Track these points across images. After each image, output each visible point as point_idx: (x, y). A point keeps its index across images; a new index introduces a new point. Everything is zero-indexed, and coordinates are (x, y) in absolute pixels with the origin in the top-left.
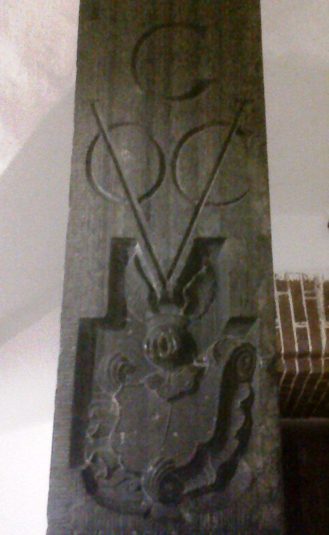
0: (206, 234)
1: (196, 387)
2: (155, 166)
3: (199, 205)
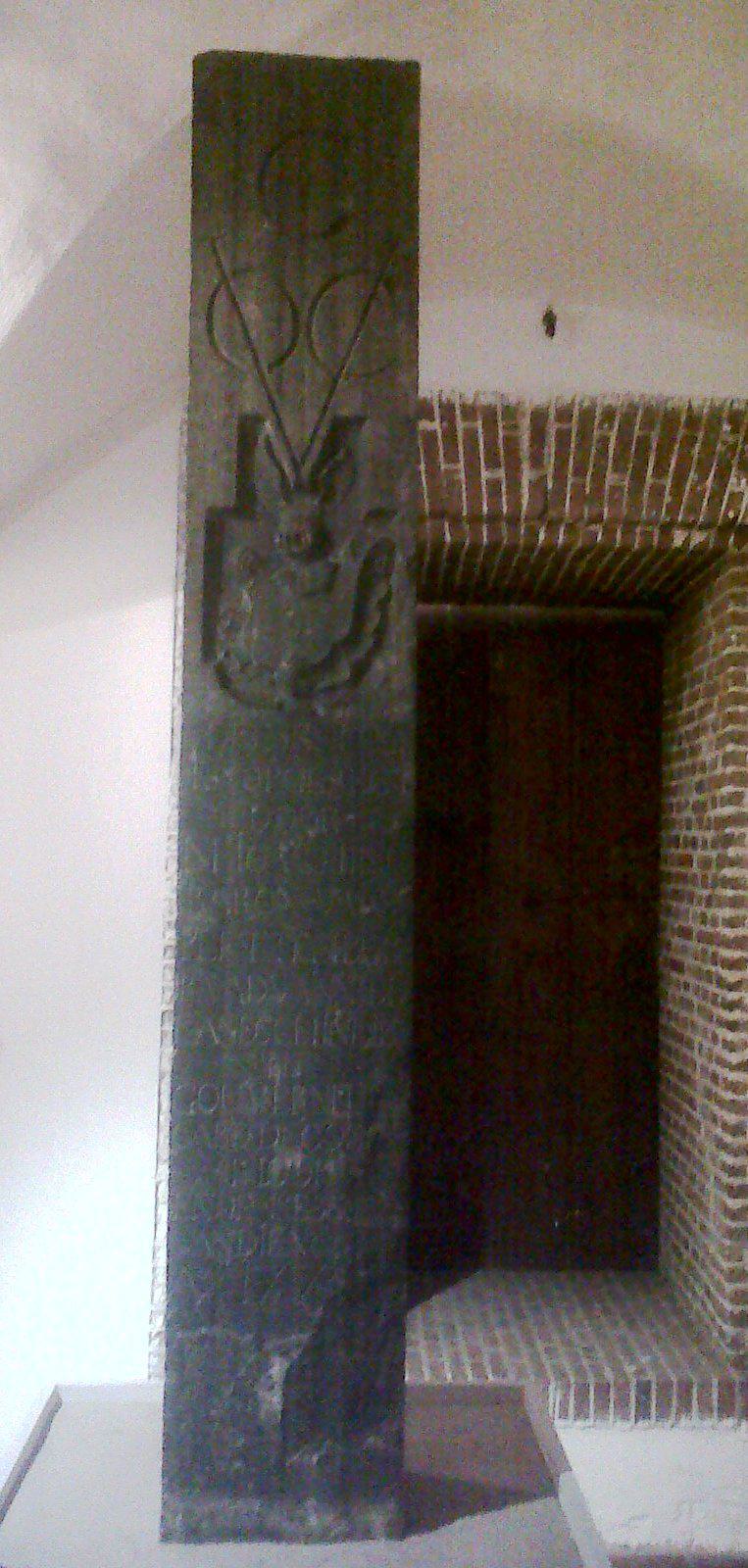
0: (345, 412)
1: (329, 587)
2: (288, 326)
3: (339, 375)
